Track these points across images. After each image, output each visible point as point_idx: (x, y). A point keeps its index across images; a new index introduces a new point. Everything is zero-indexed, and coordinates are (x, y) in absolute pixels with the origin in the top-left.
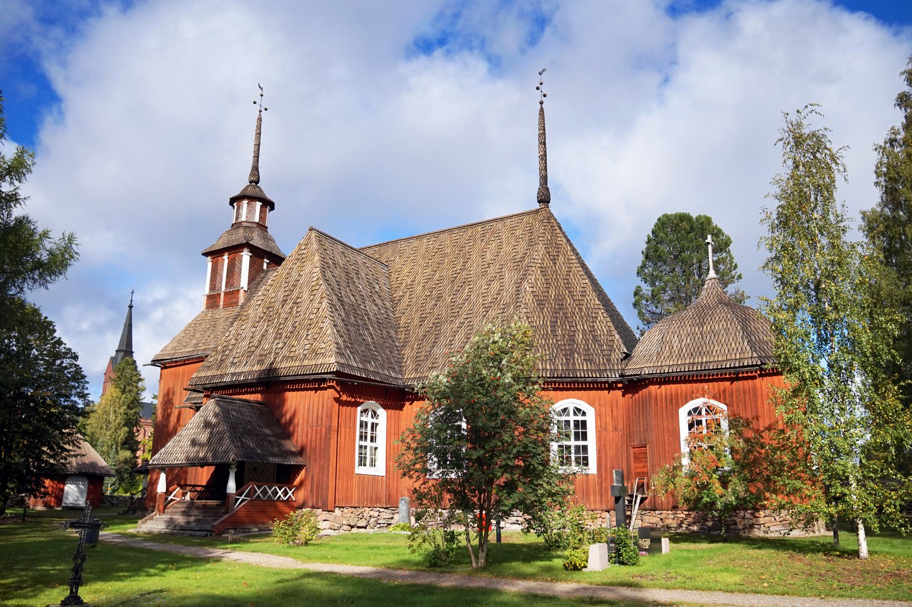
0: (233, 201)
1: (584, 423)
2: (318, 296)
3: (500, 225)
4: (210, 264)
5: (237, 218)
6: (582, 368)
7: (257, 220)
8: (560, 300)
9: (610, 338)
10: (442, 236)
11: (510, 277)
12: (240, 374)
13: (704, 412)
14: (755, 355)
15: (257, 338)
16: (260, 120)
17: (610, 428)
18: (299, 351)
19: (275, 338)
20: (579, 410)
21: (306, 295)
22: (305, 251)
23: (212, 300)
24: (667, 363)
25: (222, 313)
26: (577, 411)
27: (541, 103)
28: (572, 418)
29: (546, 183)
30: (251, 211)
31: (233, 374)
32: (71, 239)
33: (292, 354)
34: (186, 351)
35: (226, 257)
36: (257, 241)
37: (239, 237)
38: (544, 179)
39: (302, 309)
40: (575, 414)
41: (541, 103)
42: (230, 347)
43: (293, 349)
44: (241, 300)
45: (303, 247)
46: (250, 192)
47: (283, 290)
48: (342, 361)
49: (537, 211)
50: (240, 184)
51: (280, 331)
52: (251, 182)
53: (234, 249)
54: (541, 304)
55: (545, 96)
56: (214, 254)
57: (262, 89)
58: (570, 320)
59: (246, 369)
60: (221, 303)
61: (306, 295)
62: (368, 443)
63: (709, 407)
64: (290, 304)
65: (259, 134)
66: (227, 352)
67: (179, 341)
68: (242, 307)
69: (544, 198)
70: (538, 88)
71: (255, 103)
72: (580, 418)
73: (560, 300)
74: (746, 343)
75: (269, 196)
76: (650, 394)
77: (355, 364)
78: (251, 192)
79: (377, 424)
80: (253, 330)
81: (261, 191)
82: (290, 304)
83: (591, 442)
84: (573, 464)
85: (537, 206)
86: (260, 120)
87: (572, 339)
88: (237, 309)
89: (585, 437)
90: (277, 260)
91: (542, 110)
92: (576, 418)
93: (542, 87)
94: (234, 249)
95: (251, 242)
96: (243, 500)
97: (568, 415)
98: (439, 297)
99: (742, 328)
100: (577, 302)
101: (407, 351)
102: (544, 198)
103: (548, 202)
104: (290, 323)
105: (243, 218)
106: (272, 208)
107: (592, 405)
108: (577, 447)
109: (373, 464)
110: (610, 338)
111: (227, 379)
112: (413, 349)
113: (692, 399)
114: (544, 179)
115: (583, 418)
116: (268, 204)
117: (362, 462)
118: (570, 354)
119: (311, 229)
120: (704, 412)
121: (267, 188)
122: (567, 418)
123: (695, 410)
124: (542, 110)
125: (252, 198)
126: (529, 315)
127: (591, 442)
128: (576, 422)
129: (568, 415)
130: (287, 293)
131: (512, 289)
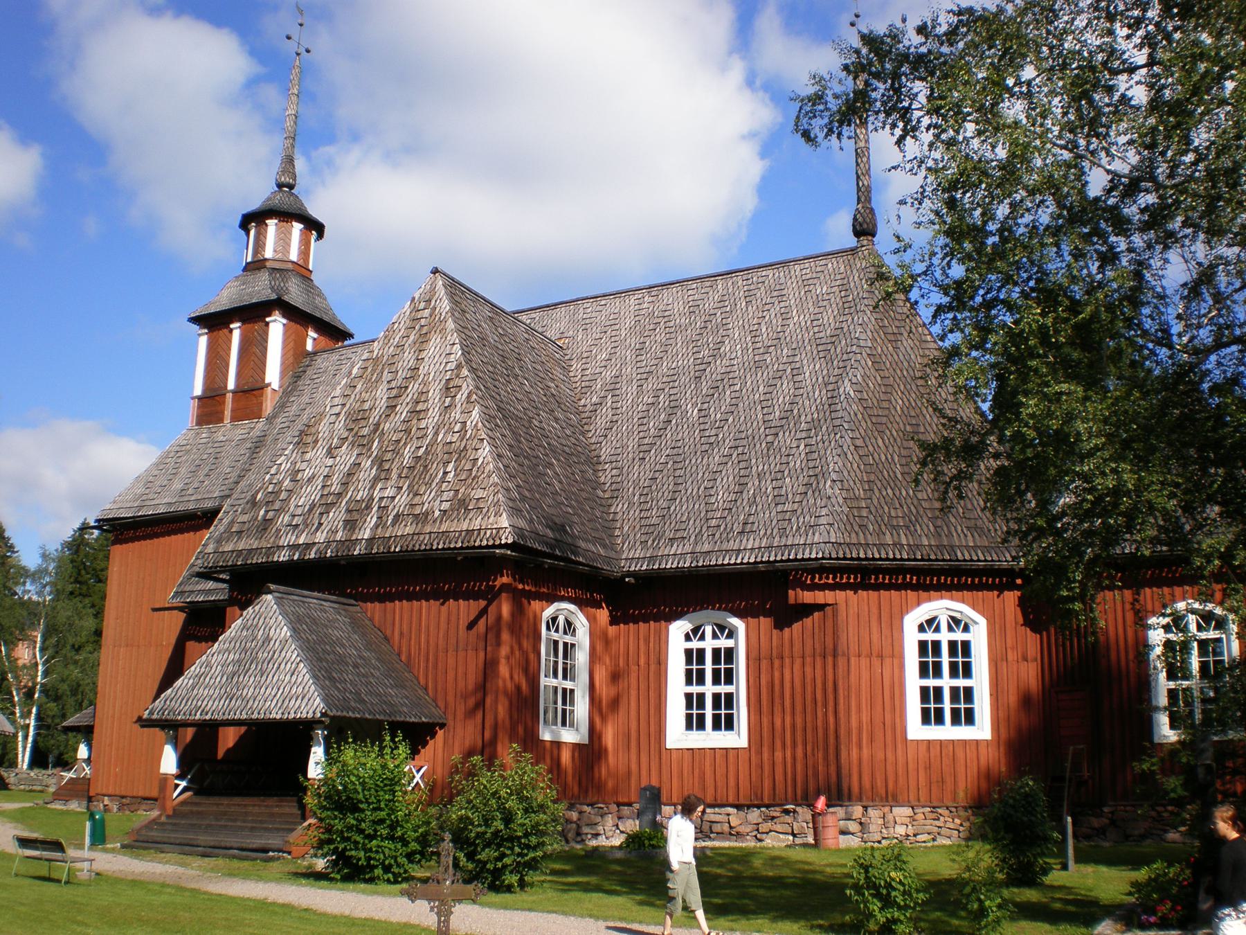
2: (461, 397)
4: (203, 341)
5: (256, 252)
7: (294, 256)
10: (666, 295)
13: (944, 626)
20: (957, 622)
25: (231, 432)
26: (955, 623)
28: (944, 637)
30: (284, 241)
31: (295, 547)
32: (743, 137)
34: (161, 504)
36: (295, 294)
37: (261, 289)
39: (432, 418)
40: (950, 629)
44: (268, 406)
45: (422, 305)
47: (383, 387)
49: (853, 251)
52: (280, 186)
53: (253, 314)
56: (214, 322)
63: (953, 618)
64: (403, 411)
66: (277, 505)
68: (271, 419)
70: (853, 24)
71: (289, 38)
72: (959, 636)
78: (281, 200)
79: (573, 645)
82: (403, 411)
83: (913, 683)
85: (851, 241)
88: (261, 425)
90: (335, 333)
94: (253, 314)
95: (286, 298)
97: (937, 630)
98: (674, 408)
101: (619, 507)
103: (874, 236)
105: (269, 253)
106: (320, 235)
108: (955, 691)
111: (283, 556)
112: (631, 504)
116: (315, 227)
119: (435, 271)
120: (944, 626)
123: (930, 622)
125: (286, 216)
126: (859, 443)
130: (394, 392)
131: (820, 395)
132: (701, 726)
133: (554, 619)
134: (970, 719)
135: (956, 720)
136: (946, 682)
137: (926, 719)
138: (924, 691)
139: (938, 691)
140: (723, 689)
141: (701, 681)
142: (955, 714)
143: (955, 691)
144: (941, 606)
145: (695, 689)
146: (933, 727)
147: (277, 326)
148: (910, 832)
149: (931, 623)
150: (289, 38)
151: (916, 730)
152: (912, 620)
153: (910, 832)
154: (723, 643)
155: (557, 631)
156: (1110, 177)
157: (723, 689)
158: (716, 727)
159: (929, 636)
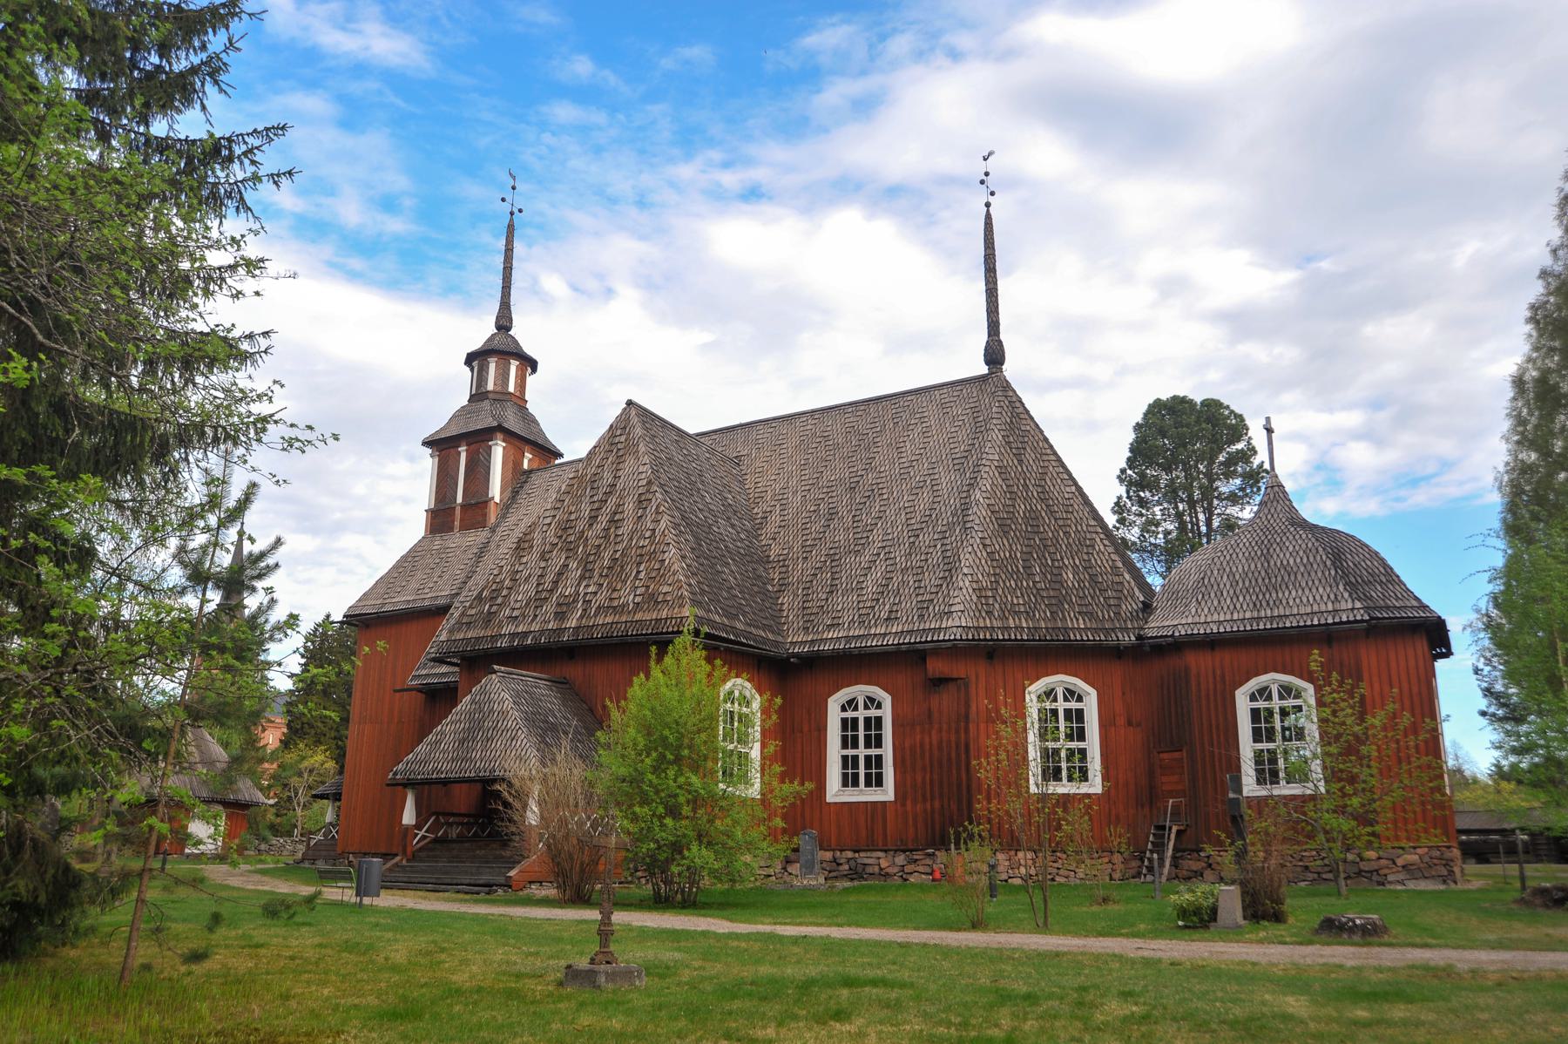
0: (470, 359)
3: (923, 399)
6: (1078, 627)
8: (1032, 518)
9: (1116, 579)
11: (947, 480)
12: (525, 634)
14: (1358, 605)
15: (550, 578)
17: (1121, 721)
18: (627, 596)
19: (582, 578)
21: (629, 506)
22: (623, 439)
23: (440, 519)
24: (1216, 617)
26: (1070, 694)
27: (988, 205)
28: (1061, 705)
29: (998, 333)
31: (513, 635)
33: (615, 603)
35: (463, 449)
36: (512, 423)
40: (866, 707)
41: (988, 205)
42: (505, 592)
43: (615, 595)
44: (492, 519)
46: (496, 344)
48: (701, 613)
50: (481, 331)
51: (590, 567)
54: (1004, 528)
55: (992, 194)
58: (1052, 550)
59: (535, 627)
60: (457, 523)
61: (629, 506)
62: (1064, 745)
64: (603, 520)
66: (499, 600)
67: (388, 582)
69: (995, 355)
70: (982, 182)
72: (1073, 705)
73: (1032, 518)
74: (1341, 587)
75: (529, 349)
76: (1187, 669)
77: (717, 619)
80: (543, 564)
81: (516, 342)
82: (603, 520)
84: (1283, 783)
85: (984, 370)
87: (1057, 581)
89: (1082, 737)
91: (988, 217)
92: (1069, 705)
93: (989, 179)
96: (424, 837)
98: (832, 514)
99: (1333, 563)
100: (1061, 522)
102: (995, 355)
104: (607, 555)
106: (534, 370)
109: (1084, 775)
110: (1116, 579)
111: (503, 643)
113: (1257, 675)
116: (530, 364)
117: (1052, 774)
118: (1057, 605)
121: (524, 333)
122: (1053, 706)
123: (850, 702)
124: (988, 217)
126: (988, 542)
128: (1068, 712)
129: (856, 709)
132: (856, 783)
134: (879, 783)
135: (868, 784)
140: (873, 752)
145: (850, 752)
154: (873, 713)
157: (873, 752)
158: (868, 784)
159: (850, 714)
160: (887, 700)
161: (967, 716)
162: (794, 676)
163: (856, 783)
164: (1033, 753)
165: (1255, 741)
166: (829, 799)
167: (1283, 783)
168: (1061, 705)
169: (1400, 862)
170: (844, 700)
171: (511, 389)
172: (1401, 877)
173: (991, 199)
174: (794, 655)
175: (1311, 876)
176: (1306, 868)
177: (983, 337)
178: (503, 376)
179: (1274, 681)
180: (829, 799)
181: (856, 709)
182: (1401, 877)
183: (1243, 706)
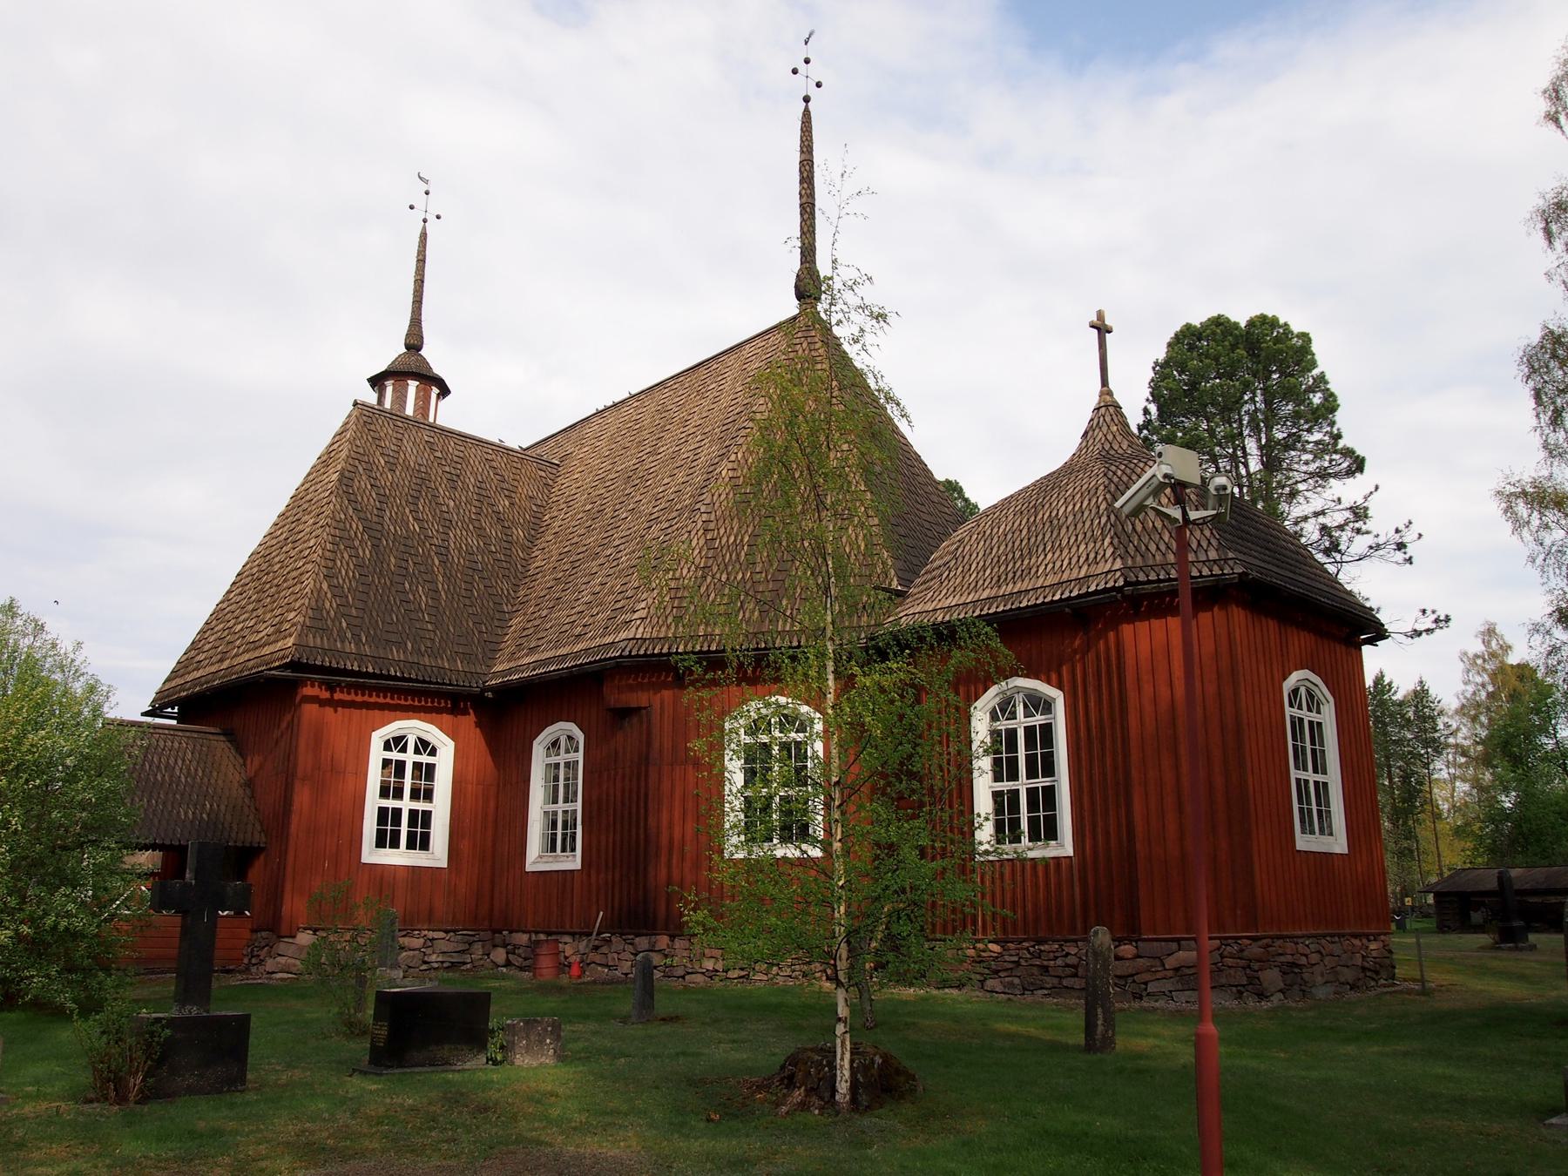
1: (431, 768)
16: (423, 237)
26: (424, 746)
27: (807, 99)
38: (808, 253)
40: (417, 751)
41: (807, 99)
50: (390, 351)
57: (426, 182)
65: (421, 261)
69: (809, 287)
71: (412, 207)
72: (424, 759)
75: (438, 369)
84: (1025, 840)
86: (423, 237)
91: (807, 114)
92: (1031, 721)
107: (1060, 688)
114: (808, 253)
115: (430, 760)
121: (435, 356)
124: (807, 114)
127: (441, 808)
128: (417, 766)
129: (404, 750)
132: (395, 844)
133: (1295, 691)
134: (425, 845)
135: (411, 845)
136: (406, 804)
137: (380, 843)
138: (383, 812)
139: (397, 813)
140: (391, 803)
141: (1013, 776)
142: (411, 838)
143: (413, 814)
144: (414, 727)
146: (388, 850)
147: (413, 385)
148: (719, 967)
149: (398, 742)
150: (412, 207)
151: (371, 854)
152: (377, 738)
153: (719, 967)
155: (1300, 708)
156: (1341, 444)
157: (391, 803)
158: (411, 845)
159: (394, 755)
160: (1058, 696)
161: (647, 758)
162: (502, 717)
163: (395, 844)
164: (983, 803)
165: (1325, 784)
166: (529, 868)
167: (1025, 840)
168: (410, 758)
169: (1170, 962)
170: (551, 739)
171: (409, 410)
172: (1167, 986)
173: (813, 92)
174: (491, 688)
175: (1050, 981)
176: (1045, 969)
177: (795, 263)
178: (400, 398)
179: (1019, 690)
180: (529, 868)
181: (404, 750)
182: (1167, 986)
183: (981, 727)
